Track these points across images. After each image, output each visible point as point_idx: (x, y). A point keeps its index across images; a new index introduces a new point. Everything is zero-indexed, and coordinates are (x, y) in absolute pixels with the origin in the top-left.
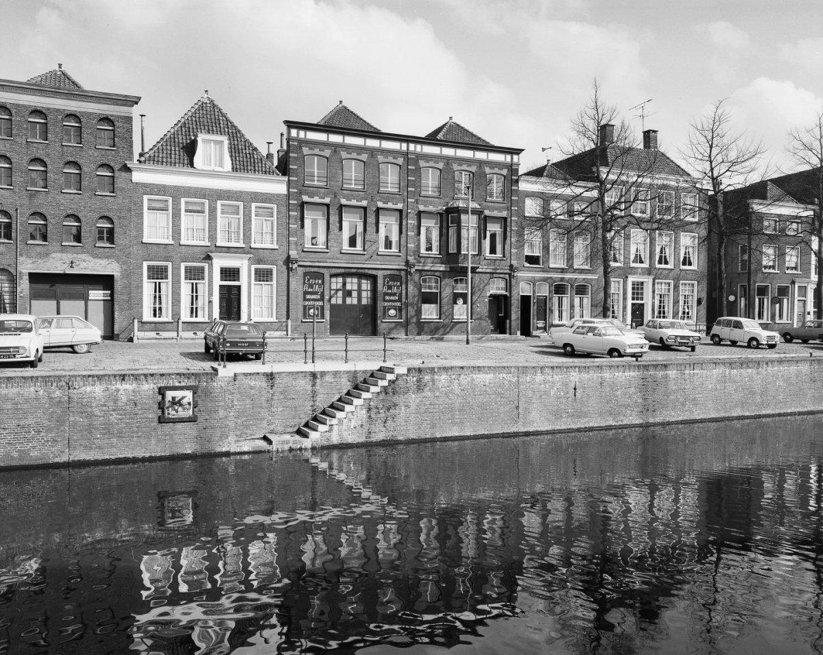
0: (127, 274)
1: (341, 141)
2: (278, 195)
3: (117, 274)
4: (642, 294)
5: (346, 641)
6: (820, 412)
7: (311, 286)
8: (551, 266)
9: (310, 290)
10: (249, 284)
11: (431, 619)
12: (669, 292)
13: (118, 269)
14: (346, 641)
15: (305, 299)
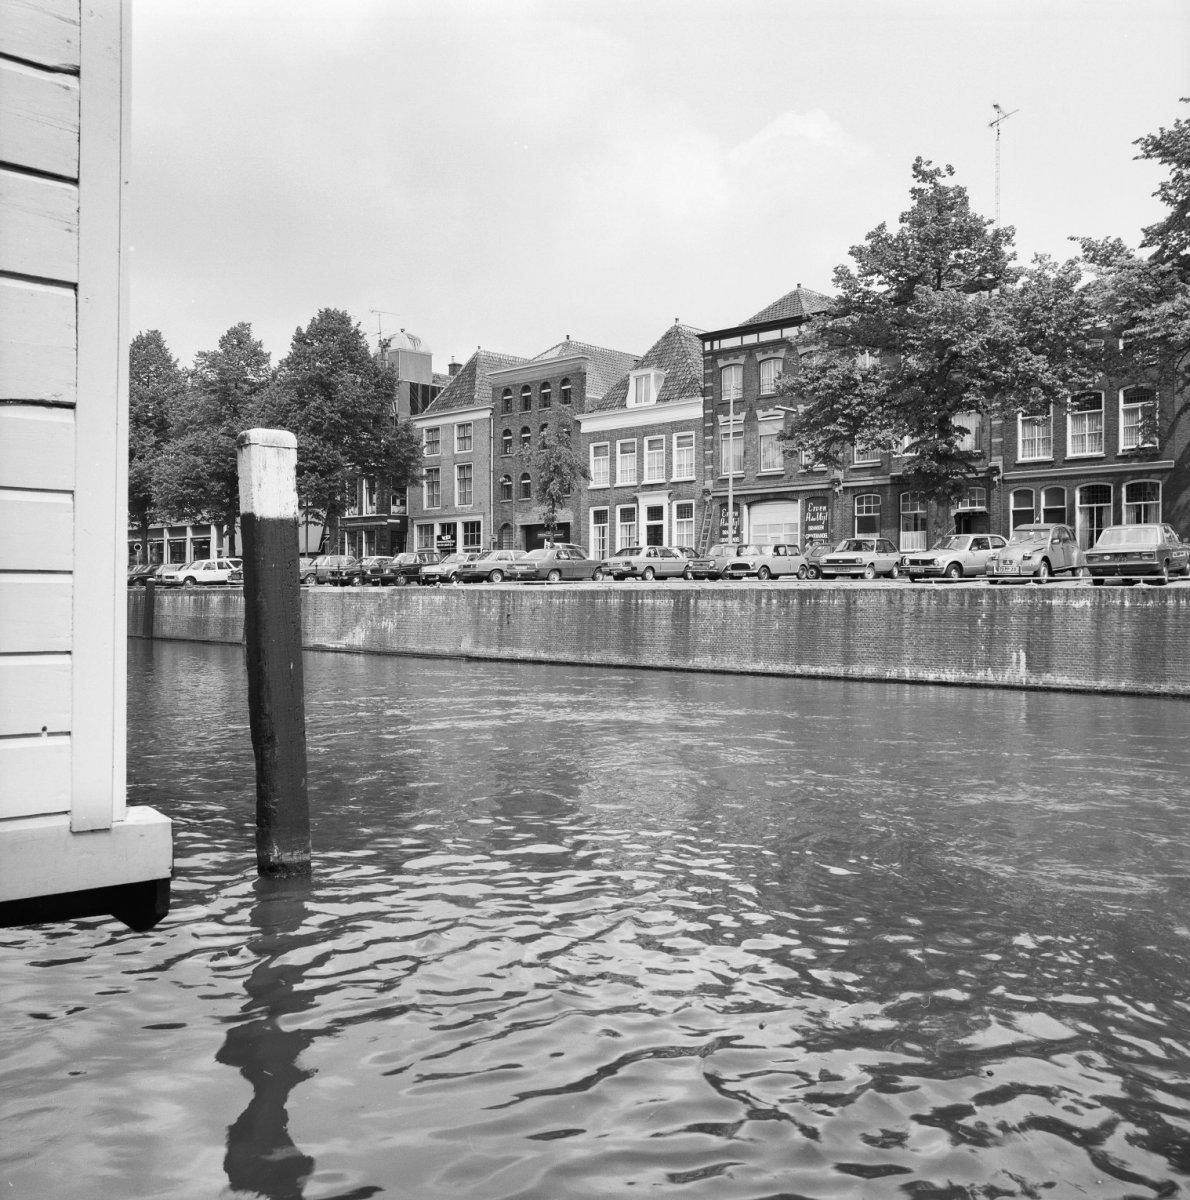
0: (577, 520)
2: (696, 420)
3: (571, 521)
5: (292, 934)
6: (5, 945)
7: (814, 514)
8: (1020, 459)
9: (813, 519)
10: (670, 521)
14: (292, 934)
15: (807, 531)
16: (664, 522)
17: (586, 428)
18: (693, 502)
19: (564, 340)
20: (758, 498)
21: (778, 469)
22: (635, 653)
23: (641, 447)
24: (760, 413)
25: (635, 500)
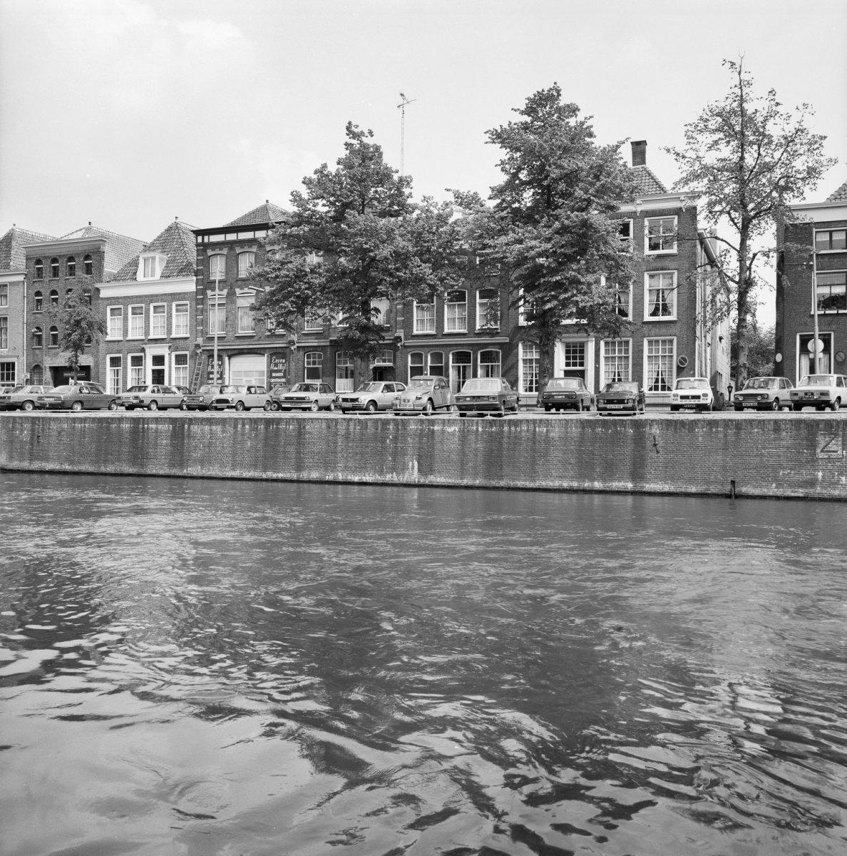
1: (239, 234)
3: (92, 365)
4: (582, 358)
11: (662, 770)
12: (672, 352)
13: (92, 361)
15: (271, 377)
16: (166, 367)
17: (103, 294)
24: (238, 291)
25: (143, 350)
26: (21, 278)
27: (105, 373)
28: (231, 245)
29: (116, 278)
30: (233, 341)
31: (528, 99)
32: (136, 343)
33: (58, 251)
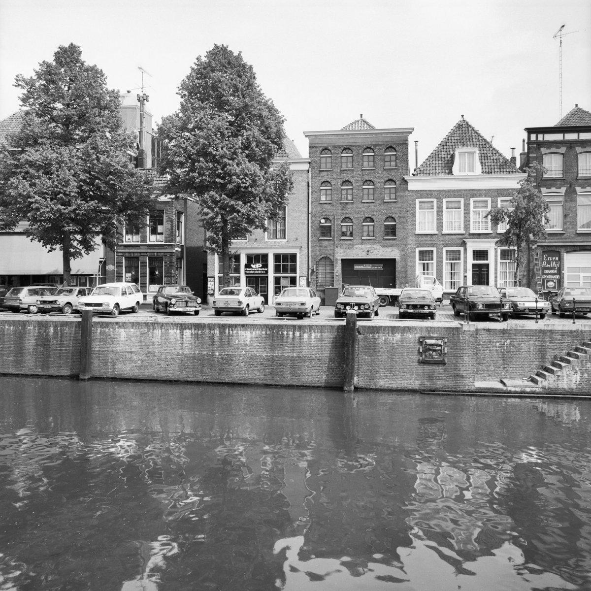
0: (404, 258)
1: (581, 134)
3: (398, 258)
7: (549, 262)
16: (491, 261)
17: (412, 186)
18: (417, 250)
19: (359, 118)
20: (578, 248)
21: (558, 229)
22: (48, 368)
23: (467, 206)
24: (579, 189)
25: (464, 244)
26: (306, 167)
27: (414, 267)
28: (571, 144)
29: (419, 172)
30: (573, 238)
31: (223, 45)
32: (454, 237)
33: (352, 141)
